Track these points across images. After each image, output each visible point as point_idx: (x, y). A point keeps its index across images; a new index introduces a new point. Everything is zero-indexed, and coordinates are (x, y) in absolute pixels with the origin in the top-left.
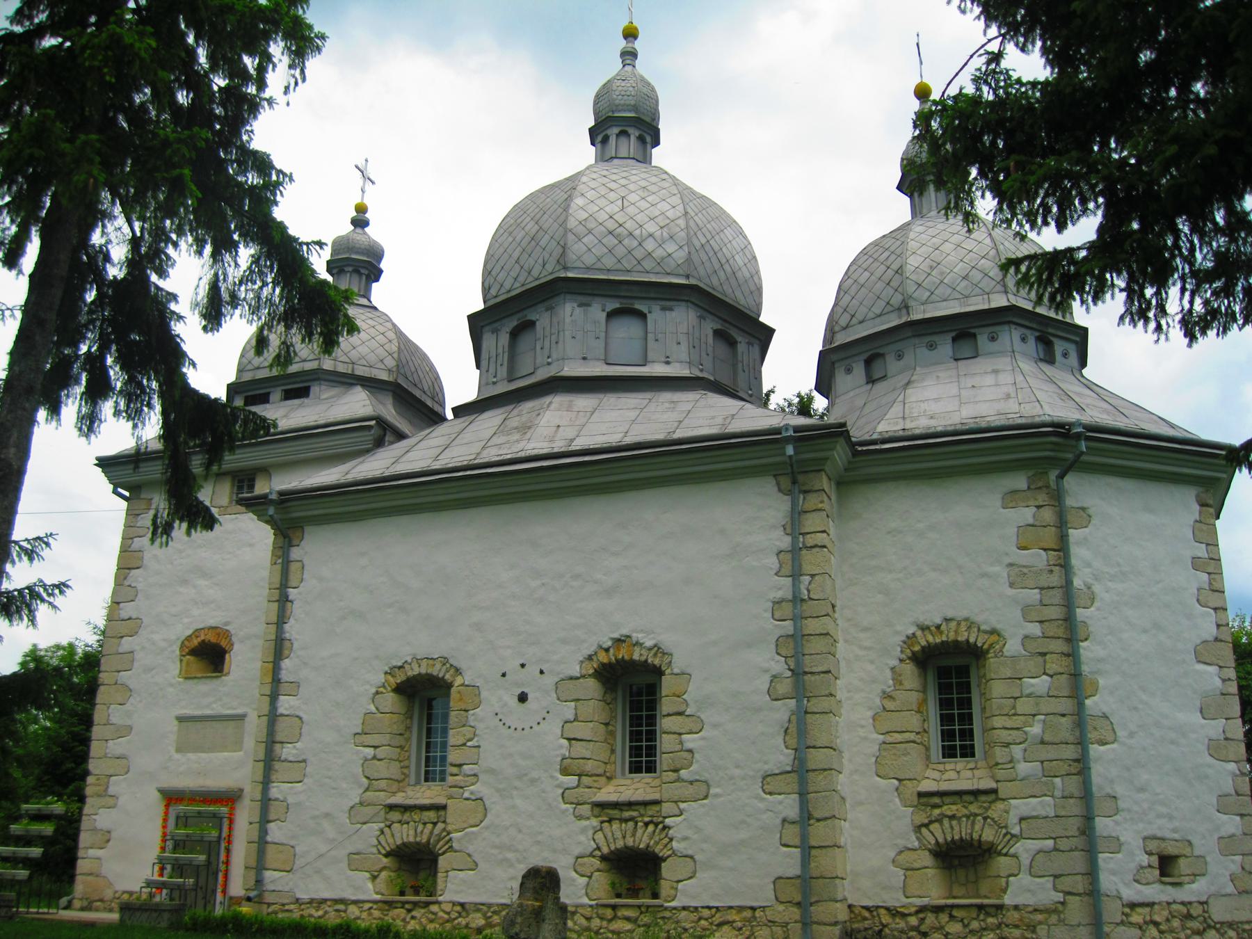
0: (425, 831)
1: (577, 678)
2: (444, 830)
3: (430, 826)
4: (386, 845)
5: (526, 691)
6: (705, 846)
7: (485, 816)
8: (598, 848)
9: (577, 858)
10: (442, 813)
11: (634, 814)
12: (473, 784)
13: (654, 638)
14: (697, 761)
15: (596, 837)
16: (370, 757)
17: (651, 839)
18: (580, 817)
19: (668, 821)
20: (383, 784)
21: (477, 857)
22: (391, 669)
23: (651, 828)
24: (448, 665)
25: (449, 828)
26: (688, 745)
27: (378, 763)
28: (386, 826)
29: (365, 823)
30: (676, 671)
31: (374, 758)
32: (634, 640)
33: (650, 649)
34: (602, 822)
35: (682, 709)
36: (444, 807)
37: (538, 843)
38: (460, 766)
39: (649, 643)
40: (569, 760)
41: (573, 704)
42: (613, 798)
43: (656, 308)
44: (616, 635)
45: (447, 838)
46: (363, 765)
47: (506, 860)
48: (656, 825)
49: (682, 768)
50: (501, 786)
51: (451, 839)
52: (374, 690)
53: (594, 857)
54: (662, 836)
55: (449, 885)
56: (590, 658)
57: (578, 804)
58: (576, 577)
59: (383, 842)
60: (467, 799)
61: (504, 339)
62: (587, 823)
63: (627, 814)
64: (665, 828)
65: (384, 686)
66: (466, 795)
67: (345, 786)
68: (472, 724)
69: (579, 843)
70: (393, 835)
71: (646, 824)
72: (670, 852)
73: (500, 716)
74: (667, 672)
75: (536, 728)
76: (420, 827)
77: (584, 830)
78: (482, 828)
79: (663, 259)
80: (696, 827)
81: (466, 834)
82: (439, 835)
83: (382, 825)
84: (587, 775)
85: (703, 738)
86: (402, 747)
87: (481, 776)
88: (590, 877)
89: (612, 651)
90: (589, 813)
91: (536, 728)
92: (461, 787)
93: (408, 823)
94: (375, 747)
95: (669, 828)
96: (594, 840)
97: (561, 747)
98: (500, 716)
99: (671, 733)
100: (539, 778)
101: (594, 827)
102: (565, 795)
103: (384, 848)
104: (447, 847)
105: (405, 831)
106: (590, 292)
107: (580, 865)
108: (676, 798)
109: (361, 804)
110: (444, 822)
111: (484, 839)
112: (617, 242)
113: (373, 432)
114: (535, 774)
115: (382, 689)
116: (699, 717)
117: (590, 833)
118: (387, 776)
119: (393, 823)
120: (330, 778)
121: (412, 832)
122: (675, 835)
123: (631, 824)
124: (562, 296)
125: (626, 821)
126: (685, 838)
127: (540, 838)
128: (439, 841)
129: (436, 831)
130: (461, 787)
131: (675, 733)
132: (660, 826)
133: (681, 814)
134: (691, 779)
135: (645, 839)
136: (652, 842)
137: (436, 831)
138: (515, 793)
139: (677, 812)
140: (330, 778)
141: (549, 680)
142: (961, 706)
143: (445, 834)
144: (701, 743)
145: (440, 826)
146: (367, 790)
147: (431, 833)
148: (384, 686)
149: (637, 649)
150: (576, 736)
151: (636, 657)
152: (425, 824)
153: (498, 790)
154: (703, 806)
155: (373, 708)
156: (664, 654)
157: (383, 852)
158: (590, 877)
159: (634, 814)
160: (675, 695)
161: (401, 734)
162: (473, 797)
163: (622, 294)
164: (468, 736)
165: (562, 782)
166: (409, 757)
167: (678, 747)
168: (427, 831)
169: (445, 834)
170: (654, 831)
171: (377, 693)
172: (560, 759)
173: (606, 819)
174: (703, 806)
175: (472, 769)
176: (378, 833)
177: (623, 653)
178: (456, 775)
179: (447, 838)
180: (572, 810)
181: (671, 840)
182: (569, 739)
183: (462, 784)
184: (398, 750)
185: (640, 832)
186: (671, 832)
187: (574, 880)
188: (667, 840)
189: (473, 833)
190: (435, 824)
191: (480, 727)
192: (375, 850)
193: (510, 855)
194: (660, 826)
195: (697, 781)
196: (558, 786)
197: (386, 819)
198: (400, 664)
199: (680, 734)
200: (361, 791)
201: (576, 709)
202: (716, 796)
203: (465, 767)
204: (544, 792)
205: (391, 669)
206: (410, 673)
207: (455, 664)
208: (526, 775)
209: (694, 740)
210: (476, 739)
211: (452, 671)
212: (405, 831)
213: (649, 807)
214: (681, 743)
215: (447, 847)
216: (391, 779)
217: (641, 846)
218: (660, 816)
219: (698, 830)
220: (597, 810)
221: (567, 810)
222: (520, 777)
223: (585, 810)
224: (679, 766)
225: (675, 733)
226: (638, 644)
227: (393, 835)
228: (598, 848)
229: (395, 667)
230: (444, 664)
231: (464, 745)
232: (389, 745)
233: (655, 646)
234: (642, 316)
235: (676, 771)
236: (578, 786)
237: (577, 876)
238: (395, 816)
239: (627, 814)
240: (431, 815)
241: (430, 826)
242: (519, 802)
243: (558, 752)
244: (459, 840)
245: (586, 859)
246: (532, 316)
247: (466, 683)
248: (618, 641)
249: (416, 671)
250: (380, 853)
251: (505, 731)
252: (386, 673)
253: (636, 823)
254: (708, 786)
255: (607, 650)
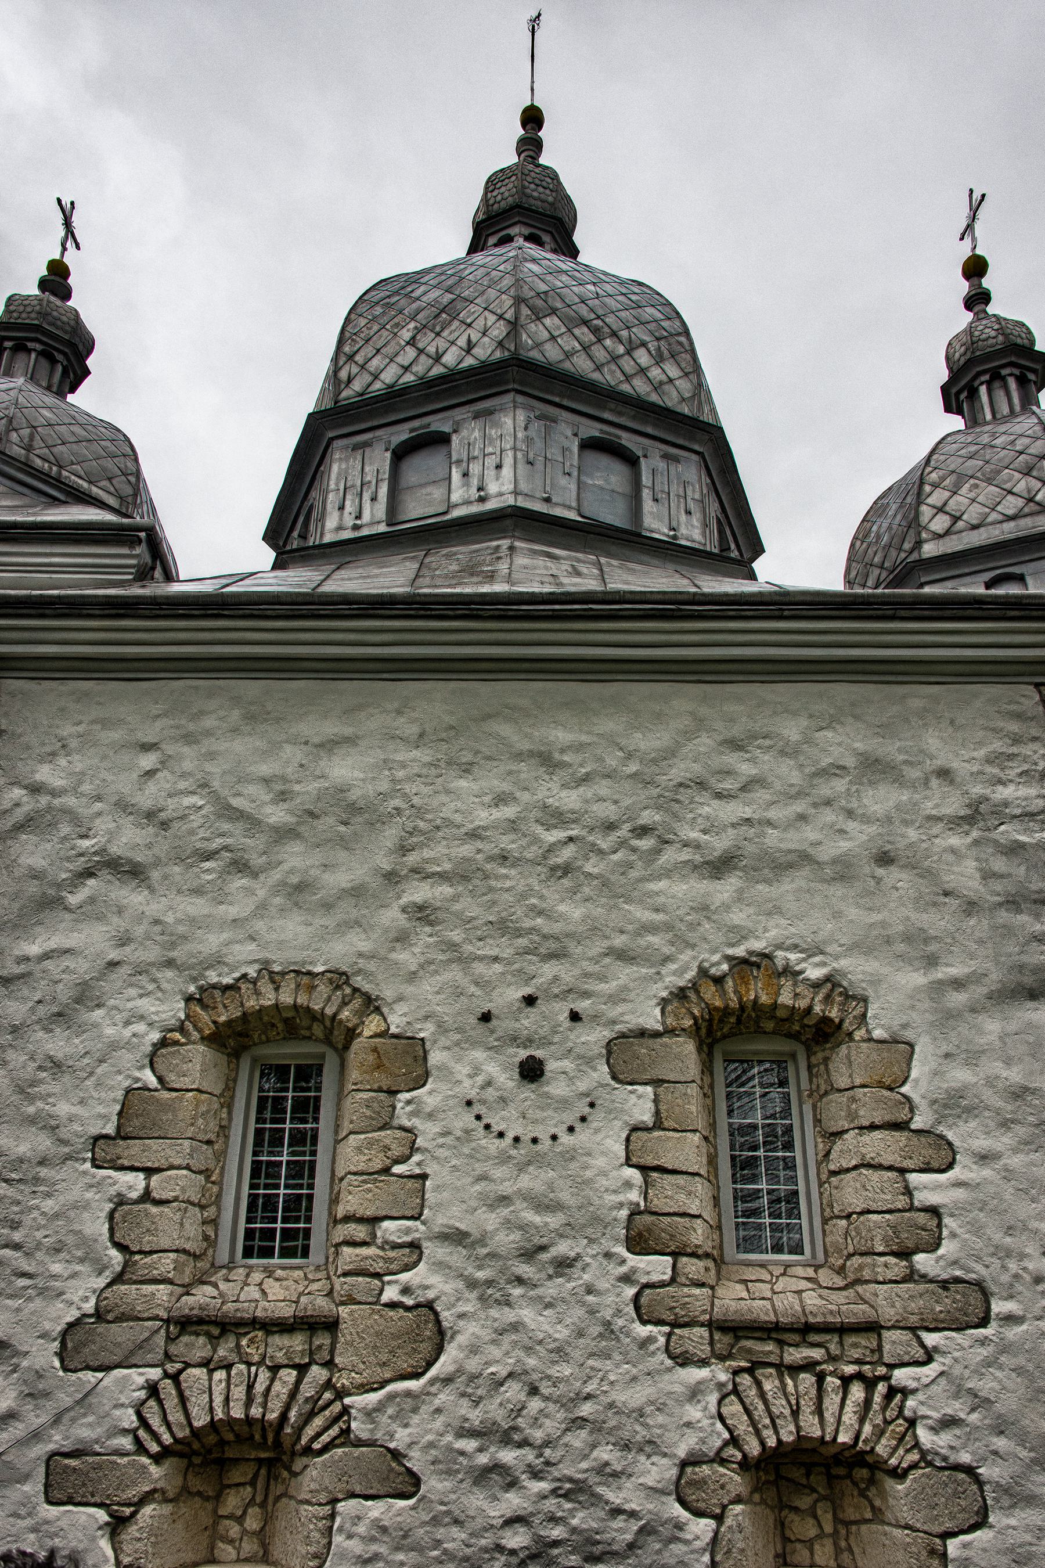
0: (277, 1386)
1: (657, 1035)
2: (328, 1385)
3: (289, 1376)
4: (162, 1430)
5: (539, 1053)
6: (1001, 1443)
7: (439, 1350)
8: (734, 1441)
9: (684, 1464)
10: (322, 1340)
11: (817, 1354)
12: (407, 1268)
13: (823, 964)
14: (953, 1235)
15: (725, 1411)
16: (134, 1195)
17: (862, 1421)
18: (683, 1360)
19: (901, 1376)
20: (166, 1263)
21: (416, 1461)
22: (202, 989)
23: (857, 1392)
24: (348, 990)
25: (342, 1380)
26: (923, 1198)
27: (154, 1210)
28: (166, 1375)
29: (107, 1368)
30: (878, 1033)
31: (146, 1197)
32: (780, 963)
33: (816, 985)
34: (736, 1372)
35: (903, 1115)
36: (332, 1325)
37: (580, 1422)
38: (375, 1220)
39: (814, 973)
40: (648, 1219)
41: (649, 1089)
42: (760, 1310)
43: (656, 449)
44: (740, 951)
45: (337, 1407)
46: (111, 1216)
47: (496, 1467)
48: (870, 1384)
49: (917, 1250)
50: (481, 1275)
51: (346, 1410)
52: (155, 1036)
53: (724, 1462)
54: (890, 1414)
55: (338, 1539)
56: (681, 994)
57: (675, 1325)
58: (643, 831)
59: (155, 1422)
60: (393, 1305)
61: (380, 460)
62: (704, 1373)
63: (795, 1355)
64: (892, 1392)
65: (181, 1029)
66: (391, 1294)
67: (56, 1268)
68: (408, 1124)
69: (688, 1425)
70: (183, 1400)
71: (846, 1381)
72: (914, 1456)
73: (477, 1109)
74: (858, 1035)
75: (565, 1139)
76: (264, 1376)
77: (694, 1393)
78: (432, 1382)
79: (661, 383)
80: (973, 1393)
81: (391, 1397)
82: (315, 1400)
83: (155, 1373)
84: (693, 1255)
85: (959, 1184)
86: (206, 1173)
87: (428, 1247)
88: (719, 1518)
89: (730, 983)
90: (704, 1350)
91: (565, 1139)
92: (377, 1275)
93: (228, 1367)
94: (149, 1172)
95: (905, 1392)
96: (721, 1418)
97: (628, 1185)
98: (477, 1109)
99: (879, 1167)
100: (578, 1257)
101: (721, 1385)
102: (643, 1300)
103: (156, 1437)
104: (334, 1431)
105: (218, 1390)
106: (557, 400)
107: (691, 1483)
108: (914, 1320)
109: (99, 1315)
110: (329, 1364)
111: (438, 1411)
112: (594, 339)
113: (138, 551)
114: (563, 1248)
115: (177, 1036)
116: (941, 1137)
117: (713, 1398)
118: (179, 1244)
119: (187, 1365)
120: (17, 1247)
121: (239, 1393)
122: (923, 1411)
123: (807, 1380)
124: (510, 397)
125: (795, 1369)
126: (949, 1422)
127: (586, 1409)
128: (312, 1415)
129: (307, 1390)
130: (377, 1275)
131: (890, 1168)
132: (881, 1388)
133: (929, 1360)
134: (945, 1276)
135: (849, 1417)
136: (867, 1429)
137: (307, 1390)
138: (517, 1291)
139: (920, 1354)
140: (17, 1247)
141: (593, 1037)
142: (270, 1202)
143: (328, 1395)
144: (960, 1194)
145: (317, 1373)
146: (118, 1279)
147: (293, 1394)
148: (181, 1029)
149: (787, 985)
150: (663, 1162)
151: (785, 998)
152: (275, 1369)
153: (472, 1284)
154: (983, 1342)
155: (152, 1081)
156: (847, 996)
157: (154, 1448)
158: (719, 1518)
159: (817, 1354)
160: (881, 1085)
161: (209, 1142)
162: (409, 1302)
163: (607, 416)
164: (396, 1151)
165: (634, 1270)
166: (219, 1196)
167: (901, 1202)
168: (281, 1389)
169: (328, 1395)
170: (868, 1402)
171: (163, 1043)
172: (624, 1213)
173: (744, 1364)
174: (983, 1342)
175: (408, 1231)
176: (142, 1394)
177: (758, 992)
178: (364, 1244)
179: (337, 1407)
180: (662, 1340)
181: (912, 1423)
182: (644, 1169)
183: (379, 1267)
184: (201, 1178)
185: (831, 1402)
186: (910, 1403)
187: (680, 1526)
188: (900, 1426)
189: (408, 1394)
190: (302, 1369)
191: (427, 1132)
192: (126, 1443)
193: (508, 1456)
194: (881, 1388)
195: (957, 1280)
196: (626, 1279)
197: (168, 1357)
198: (227, 980)
199: (902, 1171)
200: (101, 1282)
201: (656, 1101)
202: (1010, 1319)
203: (386, 1224)
204: (589, 1292)
205: (202, 989)
206: (251, 1003)
207: (367, 987)
208: (543, 1248)
209: (937, 1187)
210: (416, 1158)
211: (357, 1003)
212: (218, 1390)
213: (850, 1339)
214: (908, 1192)
215: (334, 1431)
216: (185, 1251)
217: (842, 1438)
218: (880, 1362)
219: (980, 1402)
220: (723, 1340)
221: (650, 1339)
222: (529, 1254)
223: (696, 1338)
224: (910, 1244)
225: (890, 1168)
226: (788, 972)
227: (183, 1400)
228: (734, 1441)
229: (214, 986)
230: (338, 987)
231: (386, 1171)
232: (188, 1168)
233: (828, 979)
234: (631, 461)
235: (905, 1254)
236: (673, 1280)
237: (684, 1515)
238: (197, 1347)
239: (795, 1355)
240: (297, 1342)
241: (289, 1376)
242: (527, 1314)
243: (621, 1198)
244: (370, 1414)
245: (705, 1470)
246: (439, 424)
247: (393, 1030)
248: (744, 965)
249: (269, 999)
250: (140, 1448)
251: (493, 1145)
252: (189, 999)
253: (821, 1378)
254: (986, 1297)
255: (719, 981)
